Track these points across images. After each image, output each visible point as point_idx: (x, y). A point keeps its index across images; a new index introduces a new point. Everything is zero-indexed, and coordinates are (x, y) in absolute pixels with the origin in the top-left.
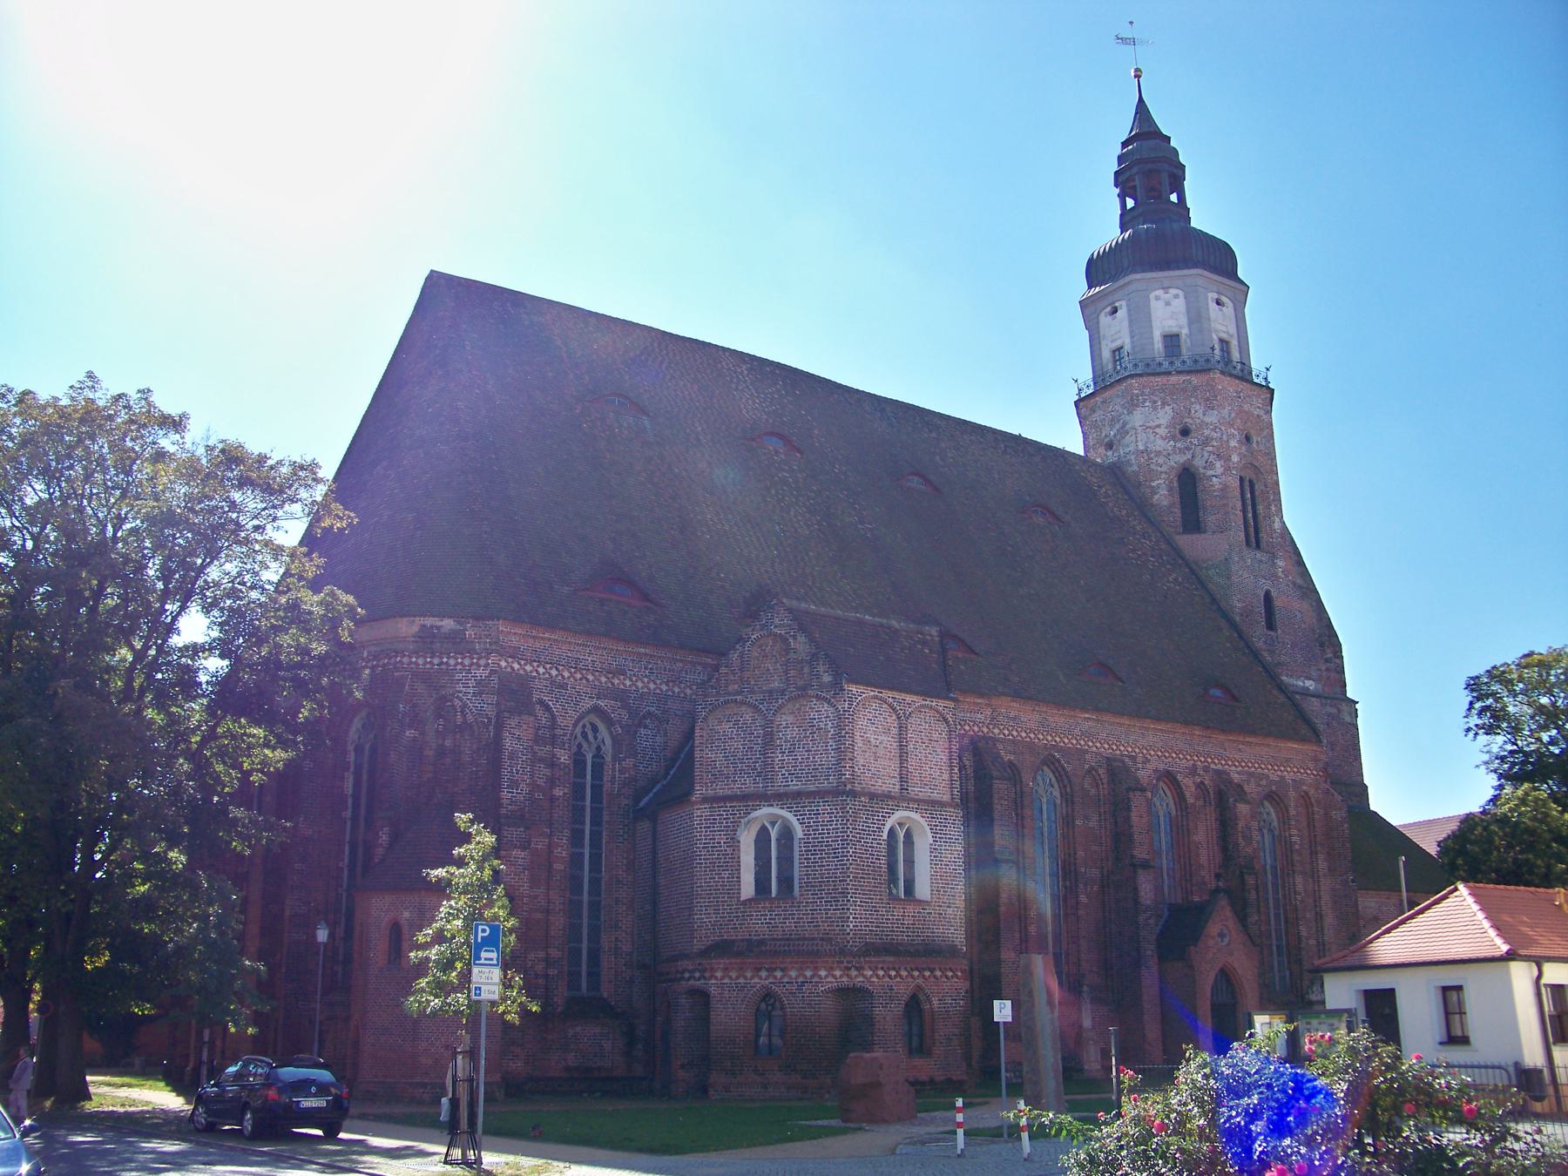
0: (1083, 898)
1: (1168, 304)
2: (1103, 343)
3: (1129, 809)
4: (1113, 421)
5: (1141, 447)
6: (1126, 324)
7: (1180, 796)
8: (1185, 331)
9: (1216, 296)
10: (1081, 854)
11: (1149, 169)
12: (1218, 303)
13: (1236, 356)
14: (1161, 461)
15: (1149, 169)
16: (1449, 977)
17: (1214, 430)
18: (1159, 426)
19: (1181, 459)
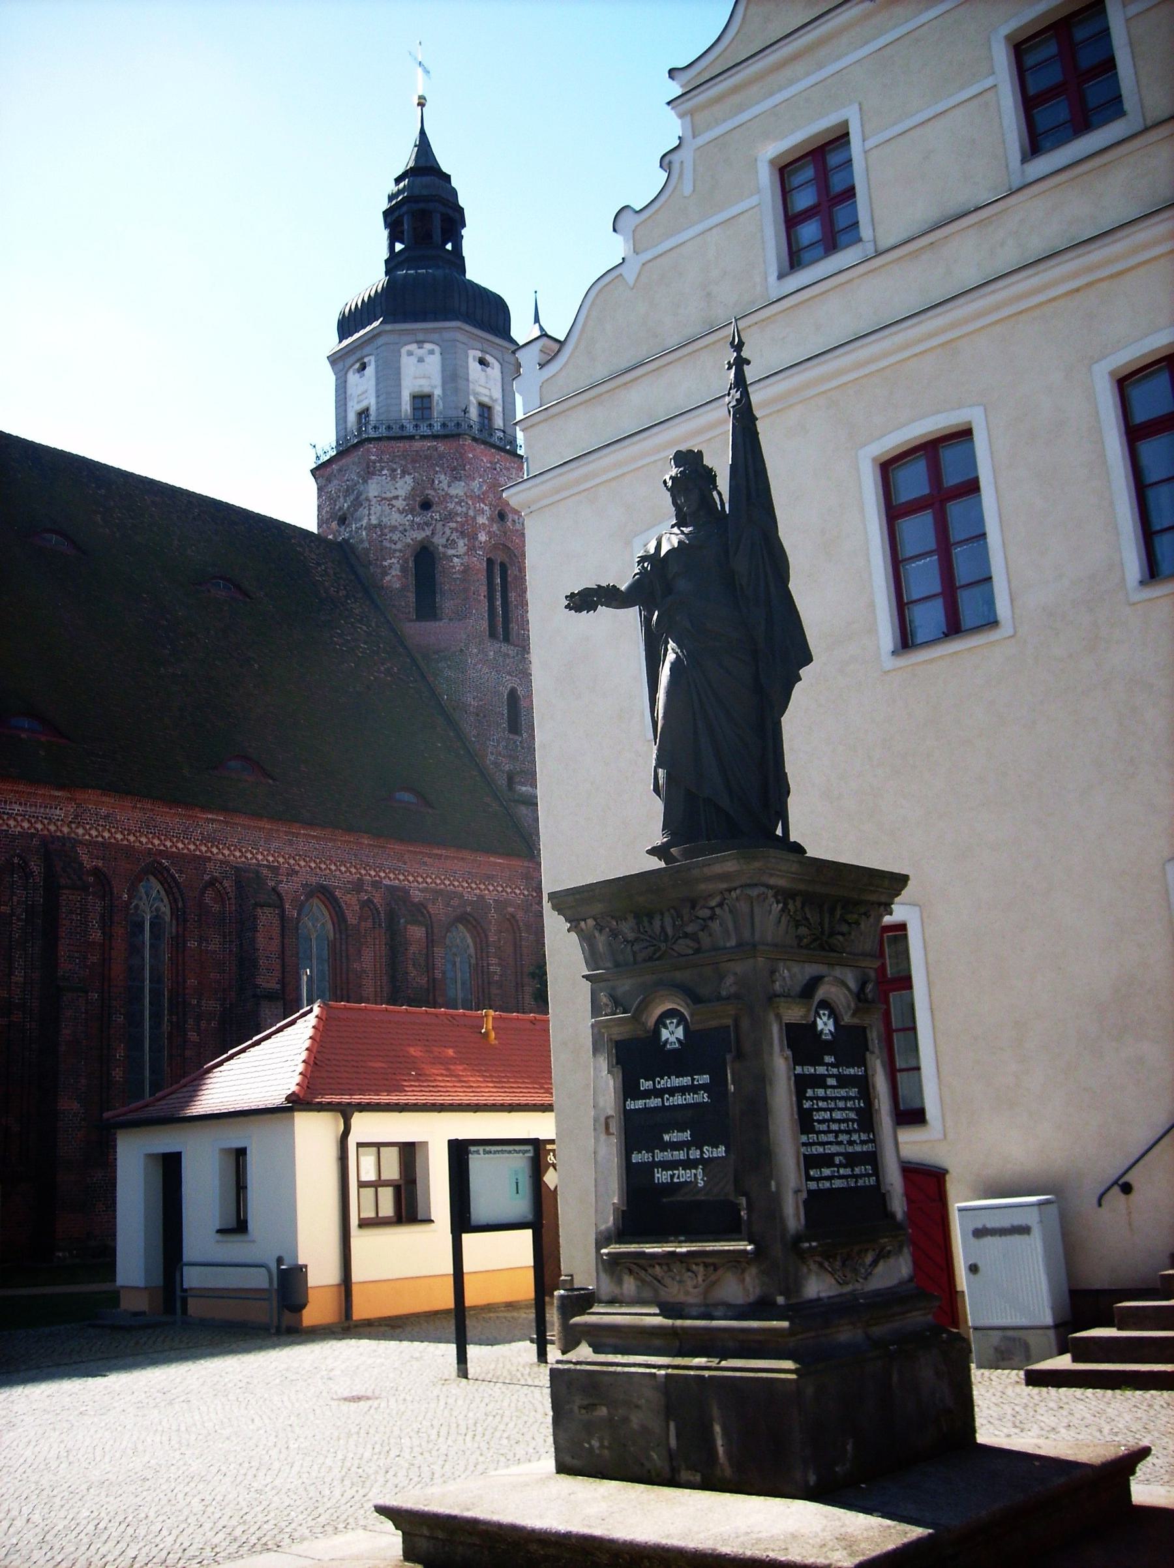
0: (193, 1036)
1: (421, 360)
2: (350, 404)
3: (255, 930)
4: (348, 492)
5: (374, 521)
6: (373, 382)
7: (338, 916)
8: (438, 392)
9: (479, 354)
10: (192, 982)
11: (425, 213)
12: (482, 362)
13: (498, 422)
14: (395, 538)
15: (425, 213)
16: (234, 1137)
17: (459, 503)
18: (396, 498)
19: (420, 535)
